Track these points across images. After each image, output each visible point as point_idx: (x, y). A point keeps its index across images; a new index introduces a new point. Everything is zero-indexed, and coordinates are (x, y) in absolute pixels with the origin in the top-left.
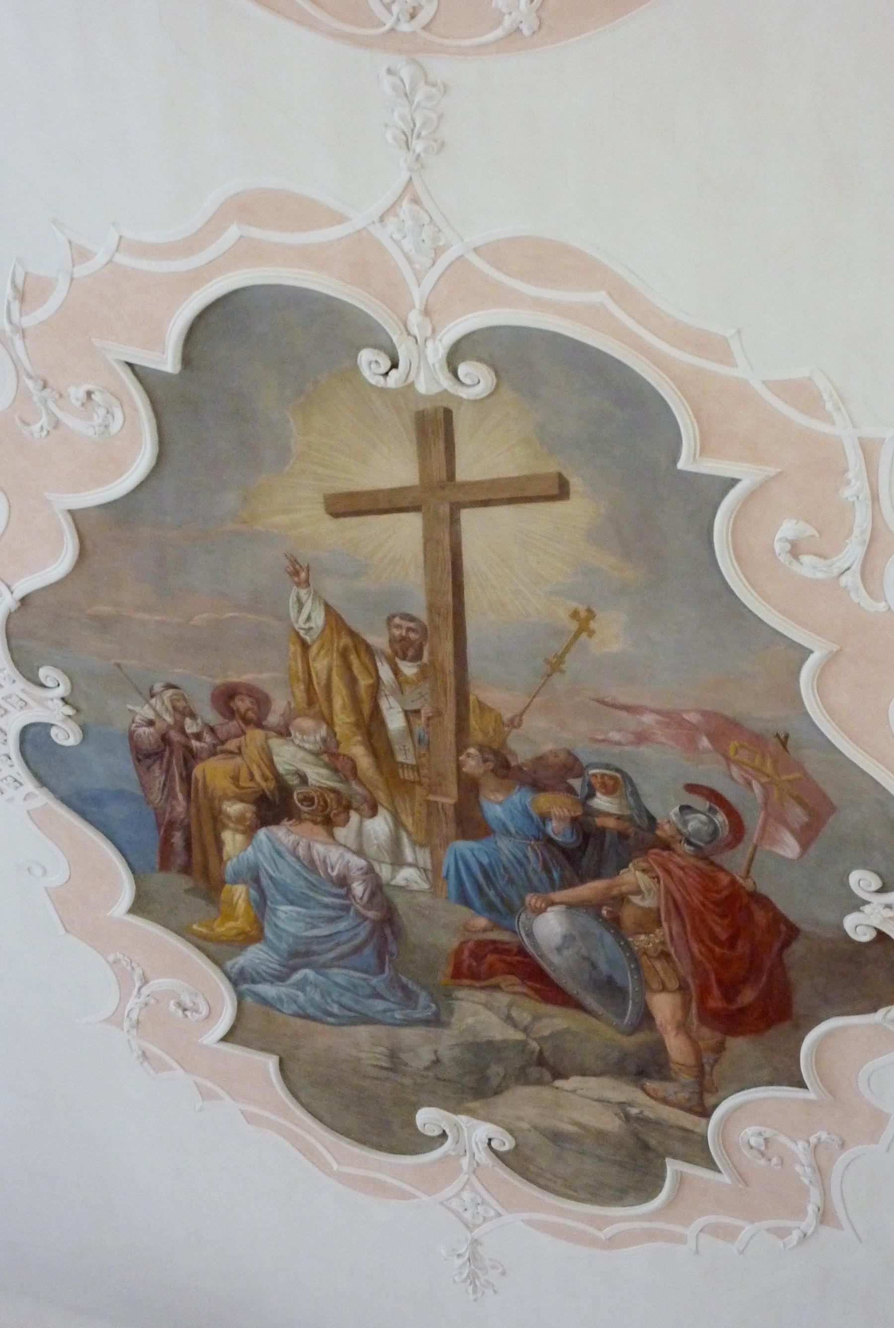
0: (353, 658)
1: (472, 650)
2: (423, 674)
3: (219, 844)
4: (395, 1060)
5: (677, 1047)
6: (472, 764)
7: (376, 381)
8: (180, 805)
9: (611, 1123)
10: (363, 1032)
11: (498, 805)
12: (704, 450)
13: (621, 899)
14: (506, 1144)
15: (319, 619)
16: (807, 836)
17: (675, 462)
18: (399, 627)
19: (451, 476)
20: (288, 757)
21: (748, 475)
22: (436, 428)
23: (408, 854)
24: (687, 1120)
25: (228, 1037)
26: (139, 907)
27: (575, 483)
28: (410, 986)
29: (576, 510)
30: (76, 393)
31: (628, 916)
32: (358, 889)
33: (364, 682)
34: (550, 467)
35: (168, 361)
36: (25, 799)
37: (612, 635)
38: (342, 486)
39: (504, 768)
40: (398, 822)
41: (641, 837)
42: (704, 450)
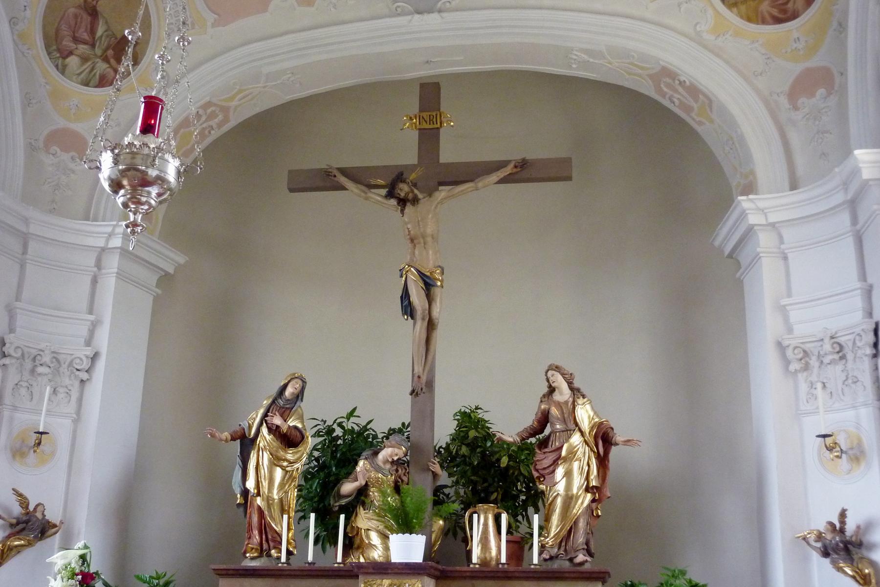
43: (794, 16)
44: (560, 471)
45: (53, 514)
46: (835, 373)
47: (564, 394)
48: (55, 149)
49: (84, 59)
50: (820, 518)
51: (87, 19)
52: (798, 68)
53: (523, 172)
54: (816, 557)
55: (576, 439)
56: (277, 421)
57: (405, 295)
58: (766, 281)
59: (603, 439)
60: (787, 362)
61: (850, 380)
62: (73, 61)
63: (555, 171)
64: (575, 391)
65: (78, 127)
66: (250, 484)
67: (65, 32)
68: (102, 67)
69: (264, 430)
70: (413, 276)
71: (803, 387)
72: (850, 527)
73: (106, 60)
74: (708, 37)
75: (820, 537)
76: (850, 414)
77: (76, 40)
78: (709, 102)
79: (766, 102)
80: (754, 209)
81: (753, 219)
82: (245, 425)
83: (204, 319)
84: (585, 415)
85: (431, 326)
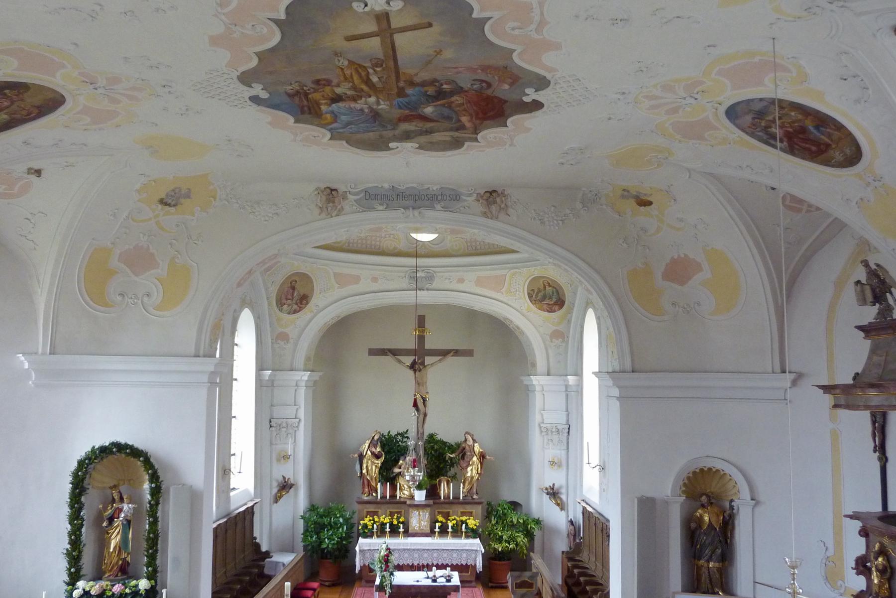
0: (360, 70)
1: (400, 62)
2: (384, 69)
3: (320, 109)
4: (381, 136)
5: (468, 125)
6: (402, 84)
7: (360, 10)
8: (305, 103)
9: (448, 139)
10: (371, 134)
11: (409, 91)
12: (482, 10)
13: (452, 102)
14: (417, 145)
15: (346, 63)
16: (511, 85)
17: (471, 14)
18: (500, 539)
19: (390, 27)
20: (338, 91)
21: (496, 15)
22: (383, 18)
23: (382, 103)
24: (474, 136)
25: (331, 139)
26: (297, 121)
27: (434, 23)
28: (595, 459)
29: (436, 29)
30: (250, 26)
31: (453, 105)
32: (366, 110)
33: (363, 74)
34: (426, 21)
35: (283, 16)
36: (650, 203)
37: (448, 54)
38: (350, 34)
39: (412, 84)
40: (378, 98)
41: (460, 91)
42: (482, 10)
43: (554, 311)
44: (469, 469)
45: (292, 481)
46: (555, 437)
47: (470, 442)
48: (279, 341)
49: (289, 305)
50: (548, 484)
51: (291, 291)
52: (555, 328)
53: (456, 353)
54: (545, 495)
55: (475, 459)
56: (374, 450)
57: (415, 401)
58: (538, 400)
59: (482, 456)
60: (541, 432)
61: (560, 441)
62: (285, 307)
63: (469, 353)
64: (474, 441)
65: (286, 330)
66: (364, 471)
67: (283, 297)
68: (295, 307)
69: (369, 452)
70: (418, 396)
71: (546, 441)
72: (556, 487)
73: (297, 304)
74: (524, 311)
75: (547, 489)
76: (558, 452)
77: (287, 299)
78: (523, 333)
79: (541, 336)
80: (537, 381)
81: (534, 383)
82: (361, 450)
83: (330, 399)
84: (477, 448)
85: (425, 415)
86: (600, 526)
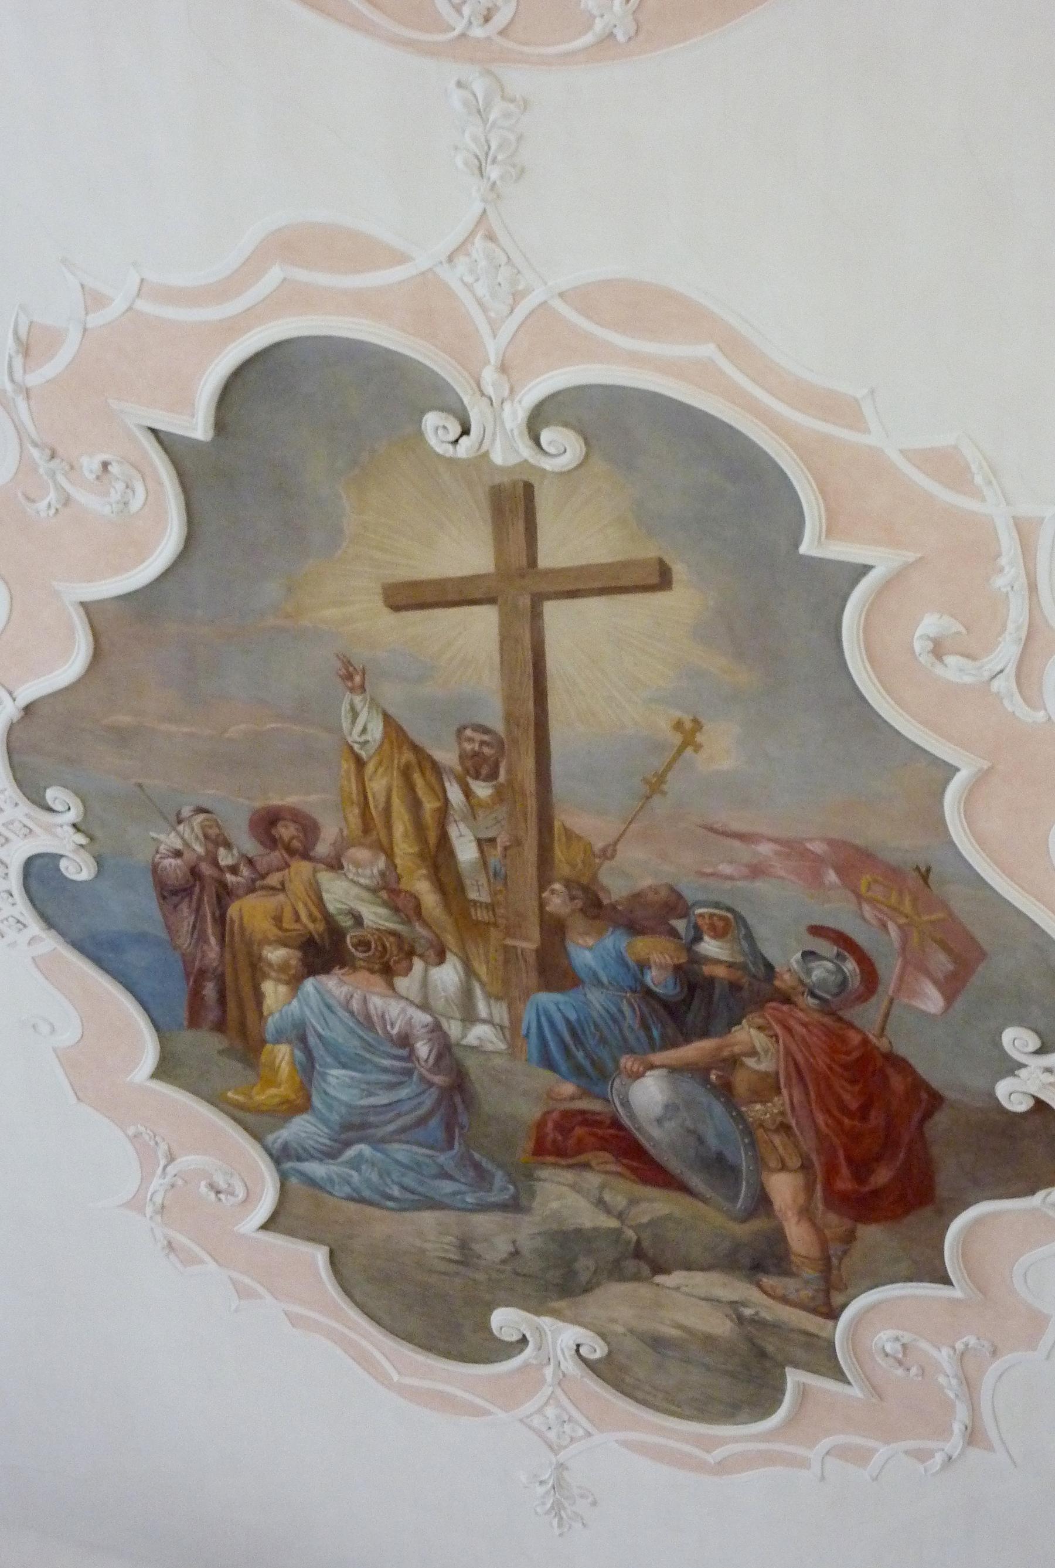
0: (417, 777)
1: (556, 768)
2: (499, 796)
3: (259, 997)
4: (466, 1252)
5: (799, 1236)
6: (557, 902)
7: (444, 449)
8: (213, 951)
9: (721, 1326)
10: (428, 1218)
11: (587, 951)
12: (831, 531)
13: (733, 1062)
14: (597, 1350)
15: (376, 731)
16: (952, 987)
17: (797, 545)
19: (533, 562)
20: (340, 893)
21: (883, 561)
22: (514, 505)
23: (482, 1008)
24: (811, 1323)
25: (269, 1225)
26: (164, 1071)
27: (679, 570)
29: (680, 602)
30: (90, 464)
31: (741, 1082)
32: (423, 1049)
33: (430, 805)
34: (649, 551)
35: (198, 426)
36: (29, 944)
37: (722, 750)
38: (404, 573)
39: (594, 906)
40: (469, 971)
41: (757, 988)
42: (831, 531)
86: (519, 952)
